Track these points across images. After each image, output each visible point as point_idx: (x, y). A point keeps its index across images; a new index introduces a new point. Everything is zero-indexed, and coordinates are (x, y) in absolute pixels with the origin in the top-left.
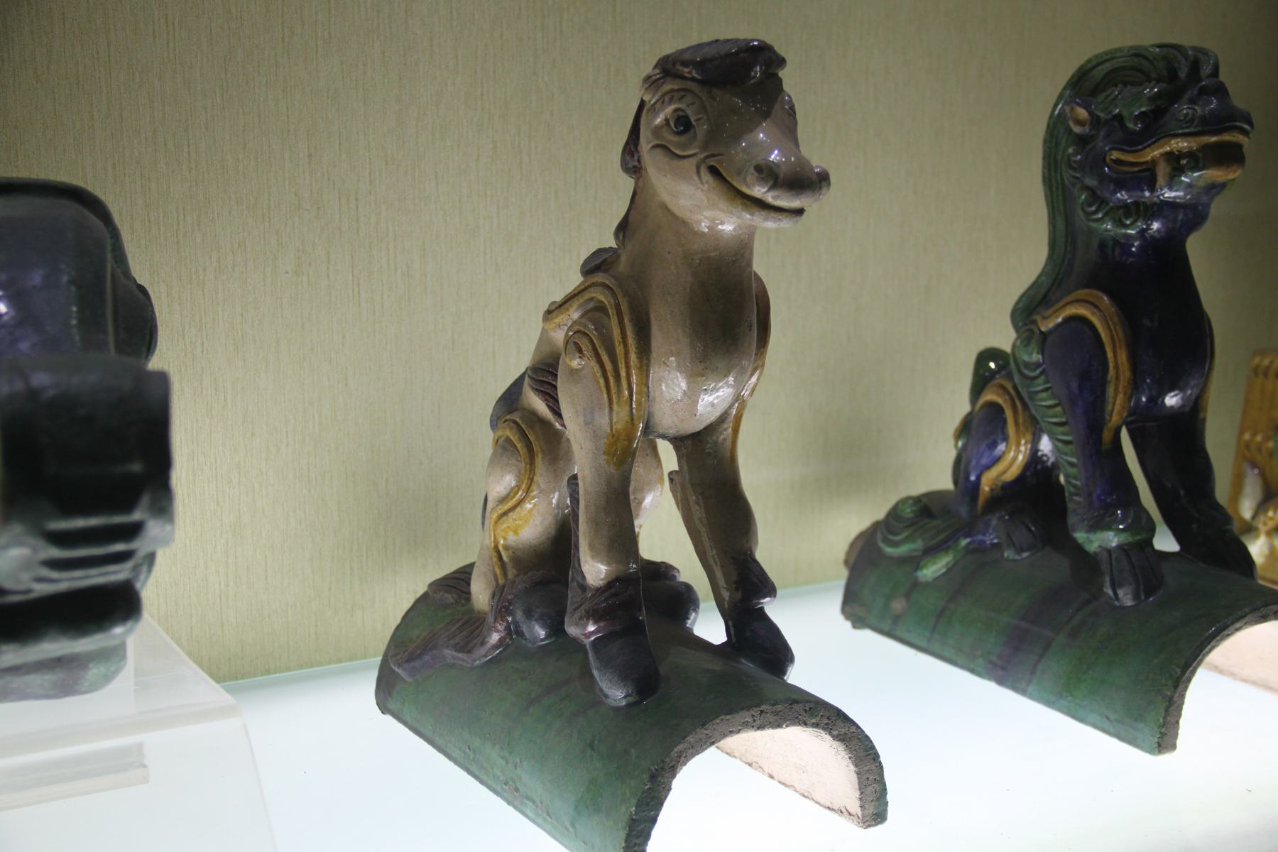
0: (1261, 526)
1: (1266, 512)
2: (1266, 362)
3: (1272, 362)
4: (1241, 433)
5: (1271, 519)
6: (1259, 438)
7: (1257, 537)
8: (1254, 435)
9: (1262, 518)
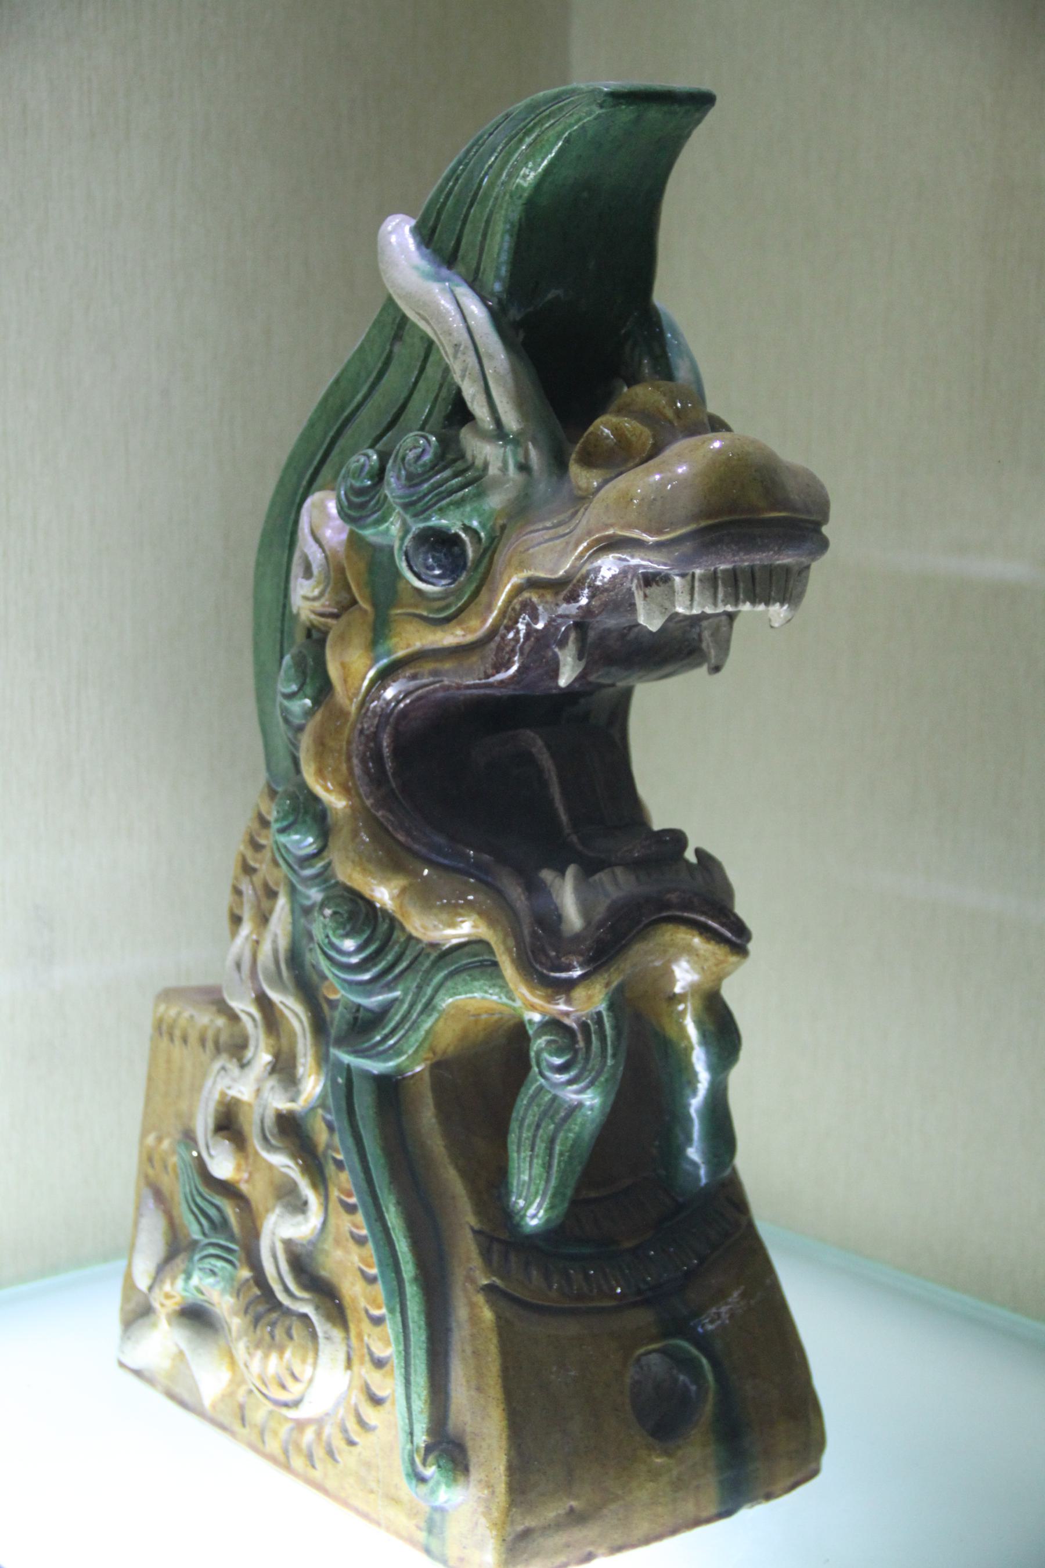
0: (156, 1305)
1: (162, 1282)
2: (173, 1012)
3: (179, 1014)
4: (144, 1134)
5: (168, 1296)
6: (166, 1144)
7: (154, 1325)
8: (160, 1140)
9: (156, 1290)
